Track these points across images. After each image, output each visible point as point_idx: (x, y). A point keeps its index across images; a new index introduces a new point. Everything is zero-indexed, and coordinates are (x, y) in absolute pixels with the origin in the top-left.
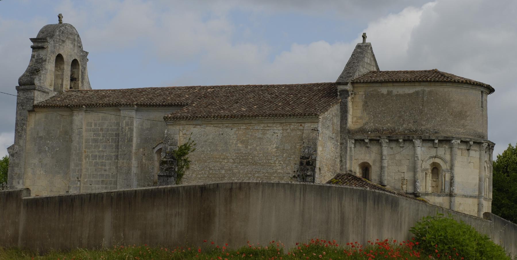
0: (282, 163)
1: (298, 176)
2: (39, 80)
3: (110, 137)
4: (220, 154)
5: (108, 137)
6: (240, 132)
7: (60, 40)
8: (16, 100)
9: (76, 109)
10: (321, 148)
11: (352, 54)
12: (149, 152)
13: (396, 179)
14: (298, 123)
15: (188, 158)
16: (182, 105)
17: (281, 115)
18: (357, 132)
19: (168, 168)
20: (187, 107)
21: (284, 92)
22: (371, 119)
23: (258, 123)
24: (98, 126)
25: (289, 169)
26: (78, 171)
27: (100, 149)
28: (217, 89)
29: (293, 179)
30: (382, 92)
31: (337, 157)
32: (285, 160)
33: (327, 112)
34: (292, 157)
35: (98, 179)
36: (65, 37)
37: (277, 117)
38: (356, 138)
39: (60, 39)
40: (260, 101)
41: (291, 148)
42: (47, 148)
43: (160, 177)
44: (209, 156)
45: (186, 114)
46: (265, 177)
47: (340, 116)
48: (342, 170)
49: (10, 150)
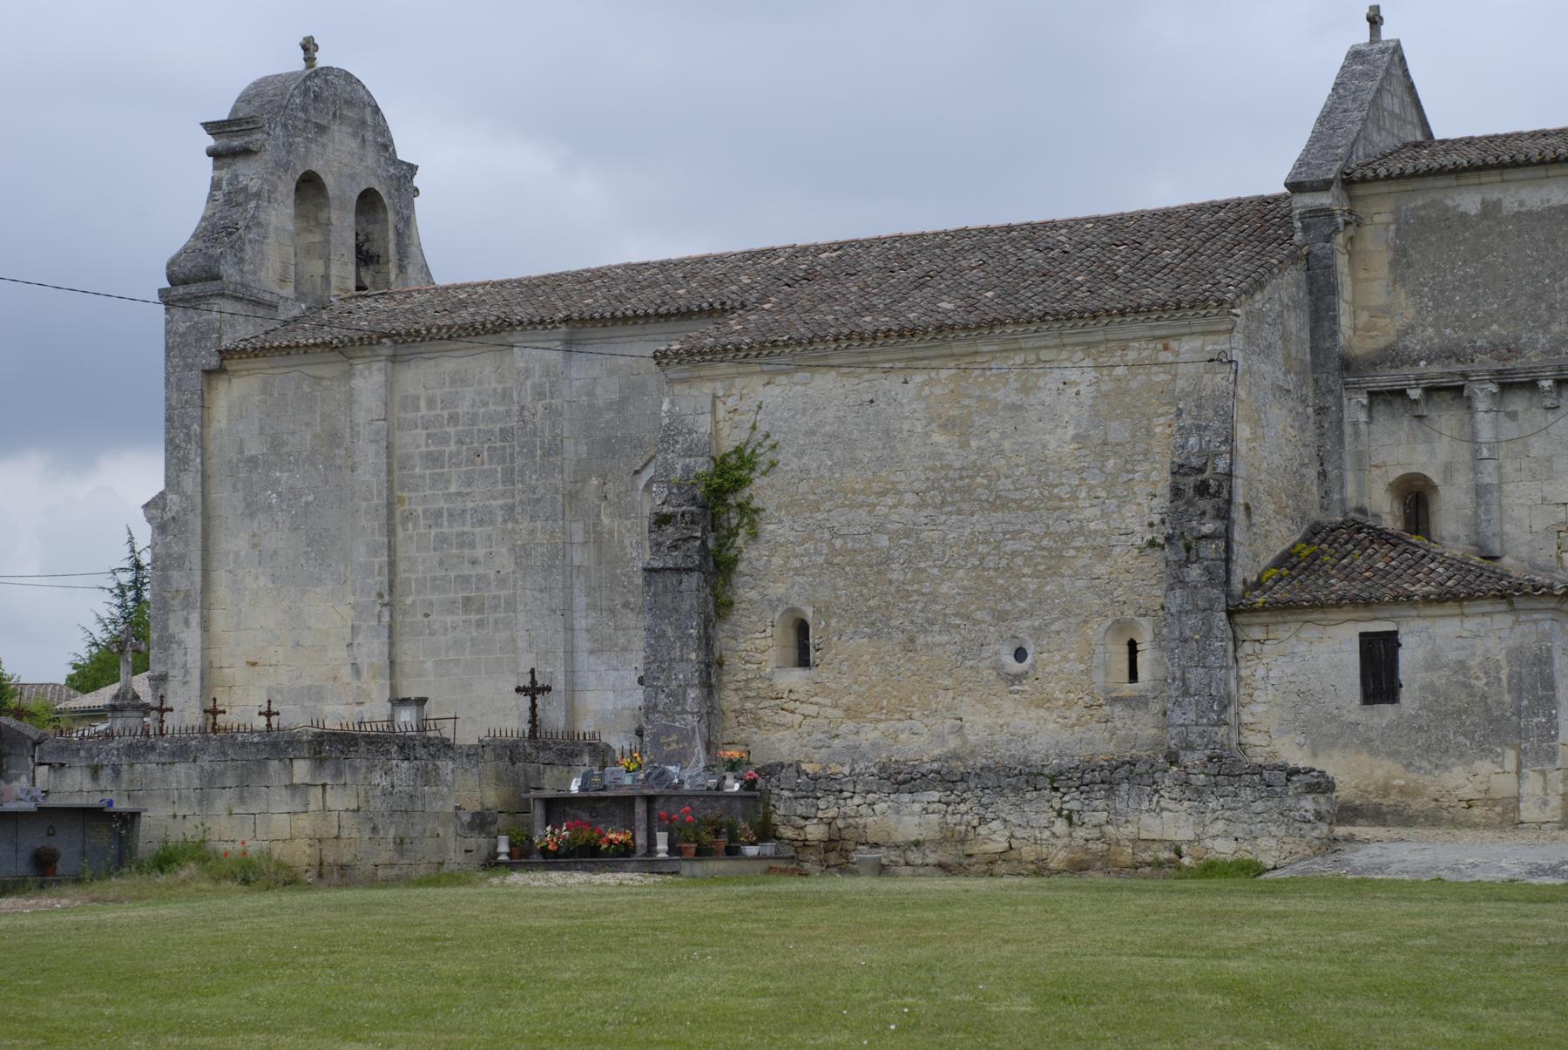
0: (1103, 494)
1: (1168, 539)
2: (238, 263)
3: (482, 443)
4: (869, 475)
5: (476, 445)
6: (938, 390)
7: (309, 124)
8: (163, 337)
9: (359, 354)
10: (1248, 430)
11: (1336, 84)
12: (623, 489)
13: (1534, 530)
14: (1154, 338)
15: (751, 496)
16: (727, 311)
17: (1086, 315)
18: (1377, 365)
19: (679, 540)
20: (740, 315)
21: (1093, 239)
22: (1424, 313)
23: (1003, 351)
24: (439, 406)
25: (1130, 515)
26: (380, 568)
27: (453, 489)
28: (852, 251)
29: (1149, 551)
30: (1461, 209)
31: (1306, 461)
32: (1113, 485)
33: (1262, 292)
34: (1137, 468)
35: (452, 595)
36: (328, 114)
37: (1073, 321)
38: (1374, 387)
39: (307, 122)
40: (1006, 274)
41: (1133, 437)
42: (275, 495)
43: (654, 574)
44: (829, 488)
45: (734, 339)
46: (1040, 553)
47: (1307, 310)
48: (1327, 510)
49: (154, 511)
